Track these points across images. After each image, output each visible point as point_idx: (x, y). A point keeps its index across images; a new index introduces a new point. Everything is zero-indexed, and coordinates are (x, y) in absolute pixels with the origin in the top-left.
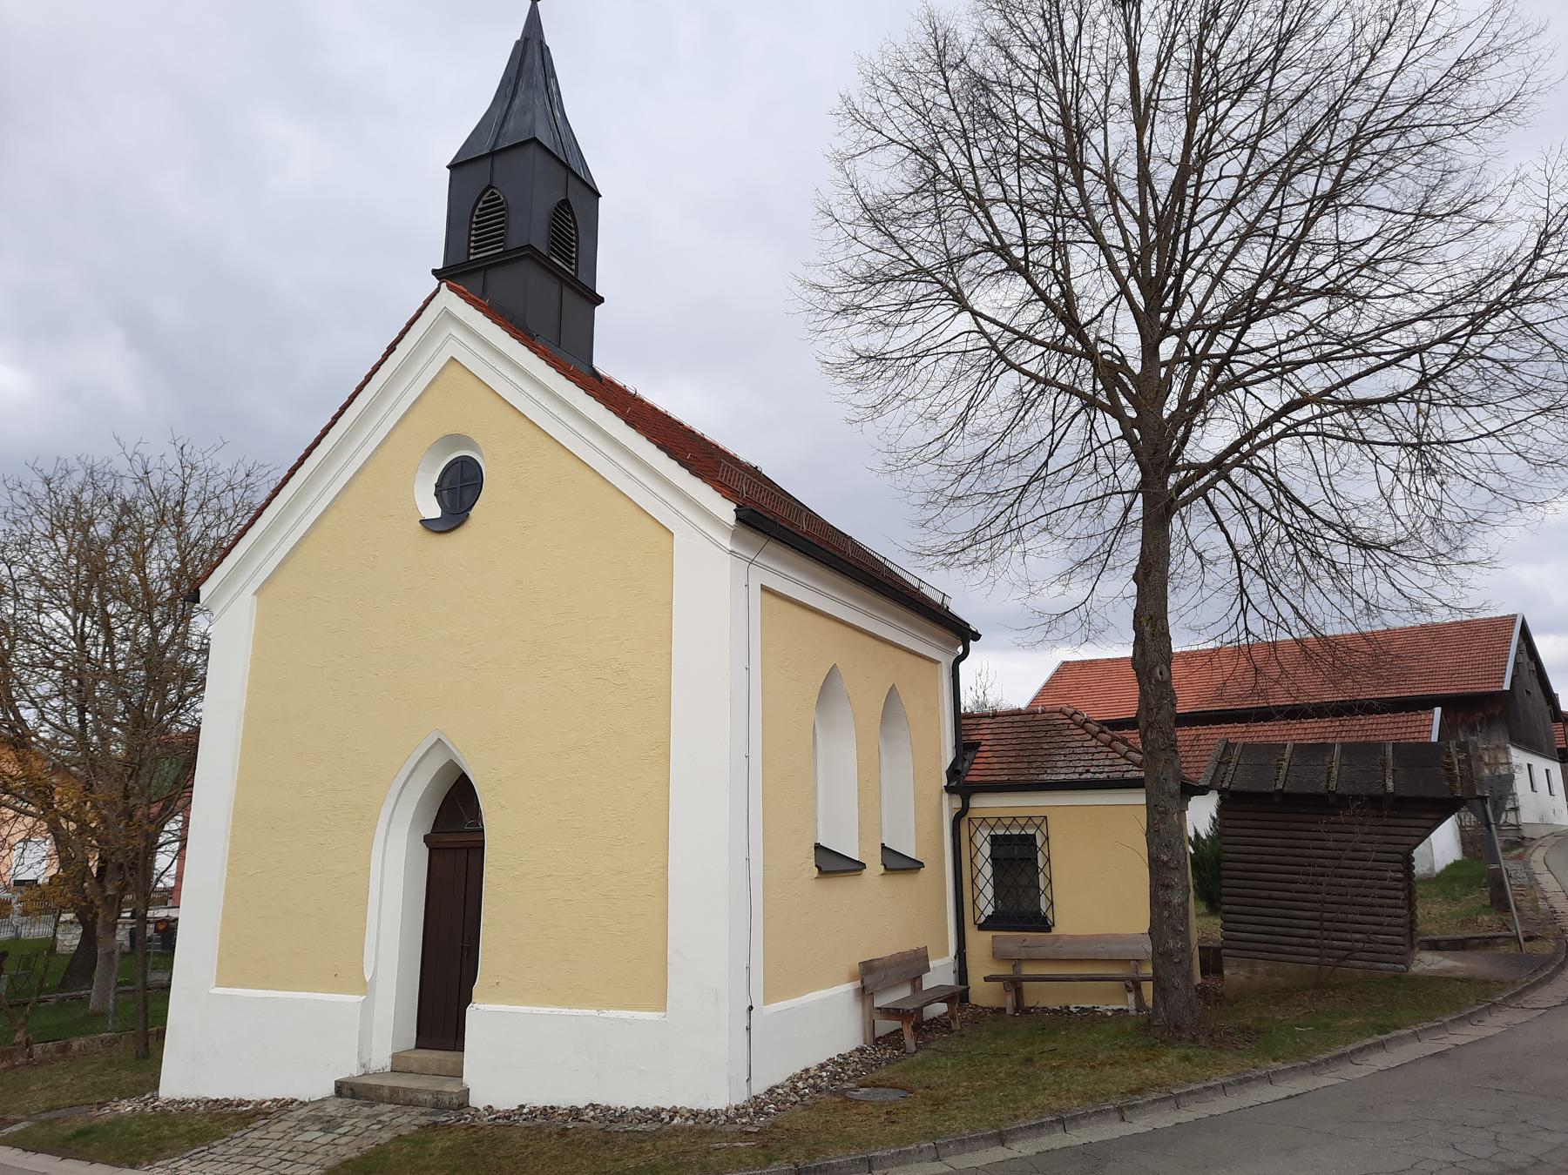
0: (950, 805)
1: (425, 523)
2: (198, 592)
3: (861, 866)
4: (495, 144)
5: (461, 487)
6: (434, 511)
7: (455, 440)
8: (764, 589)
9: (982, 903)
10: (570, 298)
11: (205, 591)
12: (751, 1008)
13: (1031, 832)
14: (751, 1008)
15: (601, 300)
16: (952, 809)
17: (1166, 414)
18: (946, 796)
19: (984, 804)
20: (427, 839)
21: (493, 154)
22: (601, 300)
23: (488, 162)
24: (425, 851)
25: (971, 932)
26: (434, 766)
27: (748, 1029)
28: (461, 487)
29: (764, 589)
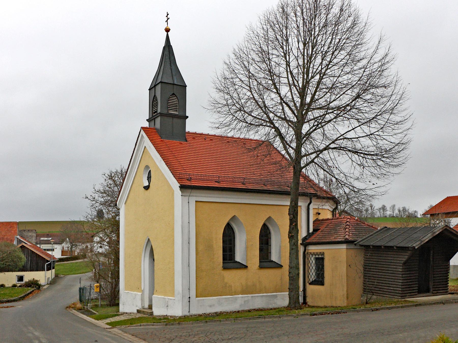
3: (280, 266)
12: (189, 298)
15: (188, 117)
19: (312, 249)
22: (188, 117)
25: (307, 285)
27: (189, 302)
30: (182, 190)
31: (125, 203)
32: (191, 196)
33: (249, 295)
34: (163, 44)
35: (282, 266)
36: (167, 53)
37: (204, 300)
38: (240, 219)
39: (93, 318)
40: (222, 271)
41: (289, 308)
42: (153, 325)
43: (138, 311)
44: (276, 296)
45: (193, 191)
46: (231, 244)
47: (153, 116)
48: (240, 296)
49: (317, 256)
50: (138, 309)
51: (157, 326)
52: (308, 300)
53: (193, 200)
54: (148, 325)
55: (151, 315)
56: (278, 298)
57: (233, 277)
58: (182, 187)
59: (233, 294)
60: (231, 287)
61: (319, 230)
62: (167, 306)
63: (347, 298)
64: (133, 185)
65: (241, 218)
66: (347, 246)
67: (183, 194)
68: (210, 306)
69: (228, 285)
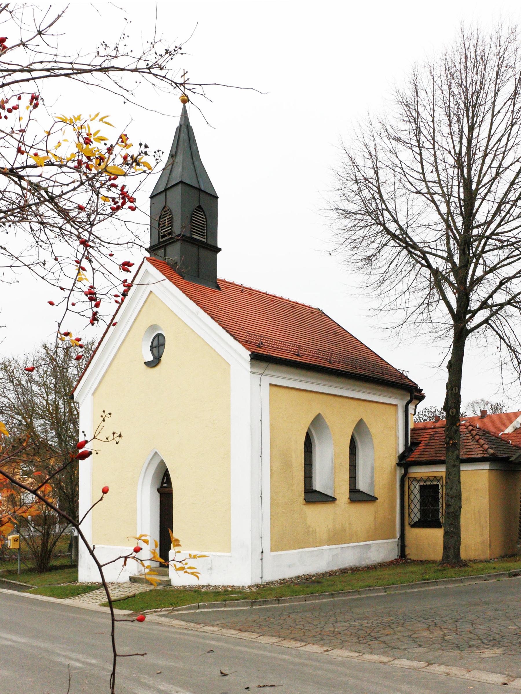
0: (400, 472)
1: (147, 364)
2: (73, 395)
3: (332, 500)
4: (167, 185)
5: (158, 345)
6: (150, 357)
7: (153, 327)
8: (271, 385)
9: (412, 516)
10: (204, 253)
11: (75, 394)
12: (262, 552)
13: (435, 483)
14: (262, 552)
15: (220, 250)
16: (400, 472)
17: (468, 286)
18: (398, 468)
19: (417, 471)
20: (158, 490)
21: (166, 190)
22: (220, 250)
23: (163, 195)
24: (158, 496)
25: (407, 527)
26: (156, 463)
27: (262, 560)
28: (158, 345)
29: (271, 385)
30: (253, 361)
31: (93, 394)
32: (266, 375)
33: (337, 546)
34: (176, 123)
35: (377, 499)
36: (184, 136)
37: (281, 555)
38: (327, 421)
39: (30, 593)
40: (304, 507)
41: (442, 563)
42: (225, 606)
43: (133, 580)
44: (369, 546)
45: (271, 366)
46: (310, 461)
47: (160, 243)
48: (327, 547)
49: (422, 484)
50: (131, 575)
51: (232, 606)
52: (407, 552)
53: (267, 380)
54: (214, 606)
55: (168, 585)
56: (373, 549)
57: (318, 516)
58: (258, 358)
59: (317, 544)
60: (315, 533)
61: (420, 443)
62: (211, 569)
63: (490, 546)
64: (116, 362)
65: (329, 418)
66: (490, 465)
67: (254, 370)
68: (290, 566)
69: (311, 530)
